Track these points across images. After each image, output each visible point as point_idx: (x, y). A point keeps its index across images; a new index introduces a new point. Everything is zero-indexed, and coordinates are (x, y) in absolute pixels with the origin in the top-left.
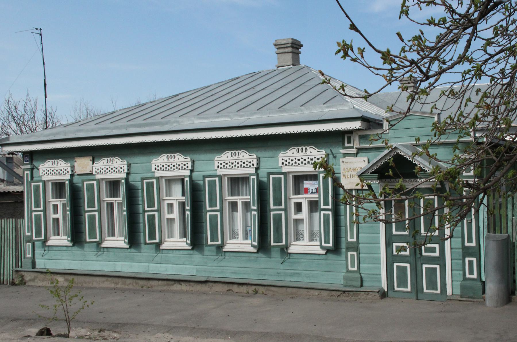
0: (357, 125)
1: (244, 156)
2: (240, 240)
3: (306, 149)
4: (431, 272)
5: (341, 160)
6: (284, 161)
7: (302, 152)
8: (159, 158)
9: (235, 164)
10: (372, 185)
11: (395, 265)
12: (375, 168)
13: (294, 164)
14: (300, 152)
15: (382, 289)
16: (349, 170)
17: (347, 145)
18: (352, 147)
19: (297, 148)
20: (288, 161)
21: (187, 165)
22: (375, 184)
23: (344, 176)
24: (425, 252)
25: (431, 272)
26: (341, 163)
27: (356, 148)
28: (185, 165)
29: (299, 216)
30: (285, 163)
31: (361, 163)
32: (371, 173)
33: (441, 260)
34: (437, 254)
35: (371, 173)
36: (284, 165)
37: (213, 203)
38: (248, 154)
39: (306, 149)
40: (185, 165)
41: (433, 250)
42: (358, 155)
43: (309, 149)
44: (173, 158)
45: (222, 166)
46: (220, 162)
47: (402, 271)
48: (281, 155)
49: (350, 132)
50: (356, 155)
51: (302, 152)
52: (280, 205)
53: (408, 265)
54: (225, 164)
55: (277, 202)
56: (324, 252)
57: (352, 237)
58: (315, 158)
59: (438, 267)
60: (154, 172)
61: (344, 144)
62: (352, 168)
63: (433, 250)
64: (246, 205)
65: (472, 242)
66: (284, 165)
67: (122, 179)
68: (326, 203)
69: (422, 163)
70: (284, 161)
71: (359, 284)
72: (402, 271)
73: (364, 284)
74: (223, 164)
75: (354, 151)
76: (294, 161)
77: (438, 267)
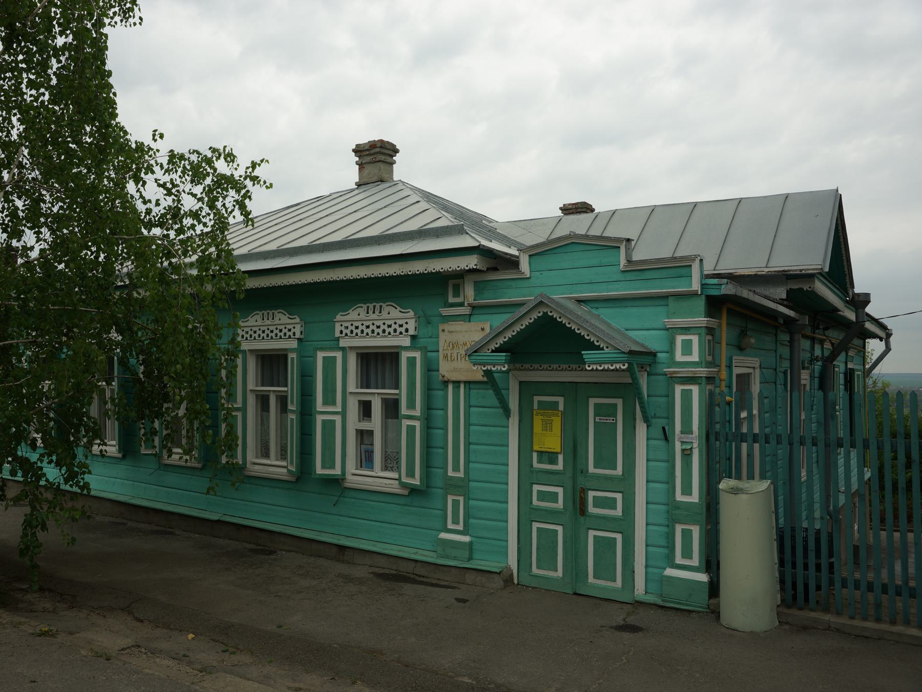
0: (471, 262)
1: (392, 313)
2: (378, 471)
3: (381, 307)
4: (605, 546)
5: (441, 328)
6: (343, 328)
7: (374, 312)
8: (350, 311)
9: (267, 332)
10: (495, 375)
11: (535, 526)
12: (501, 341)
13: (359, 334)
14: (371, 312)
15: (509, 568)
16: (454, 345)
17: (451, 300)
18: (461, 305)
19: (365, 306)
20: (382, 327)
21: (405, 326)
22: (501, 372)
23: (446, 357)
24: (595, 506)
25: (605, 546)
26: (441, 334)
27: (470, 305)
28: (401, 326)
29: (365, 426)
30: (345, 331)
31: (472, 332)
32: (493, 351)
33: (625, 525)
34: (619, 512)
35: (493, 351)
36: (386, 334)
37: (329, 399)
38: (399, 308)
39: (381, 307)
40: (401, 326)
41: (612, 504)
42: (472, 318)
43: (278, 316)
44: (377, 312)
45: (248, 336)
46: (345, 324)
47: (548, 538)
48: (338, 317)
49: (460, 275)
50: (468, 318)
51: (374, 312)
52: (334, 403)
53: (560, 529)
54: (374, 327)
55: (329, 399)
56: (406, 492)
57: (456, 468)
58: (395, 323)
59: (619, 537)
60: (338, 339)
61: (445, 295)
62: (462, 340)
63: (612, 504)
64: (283, 401)
65: (690, 494)
66: (386, 334)
67: (292, 350)
68: (411, 405)
69: (593, 334)
70: (343, 328)
71: (466, 554)
72: (548, 538)
73: (475, 556)
74: (394, 326)
75: (465, 310)
76: (394, 326)
77: (619, 537)
